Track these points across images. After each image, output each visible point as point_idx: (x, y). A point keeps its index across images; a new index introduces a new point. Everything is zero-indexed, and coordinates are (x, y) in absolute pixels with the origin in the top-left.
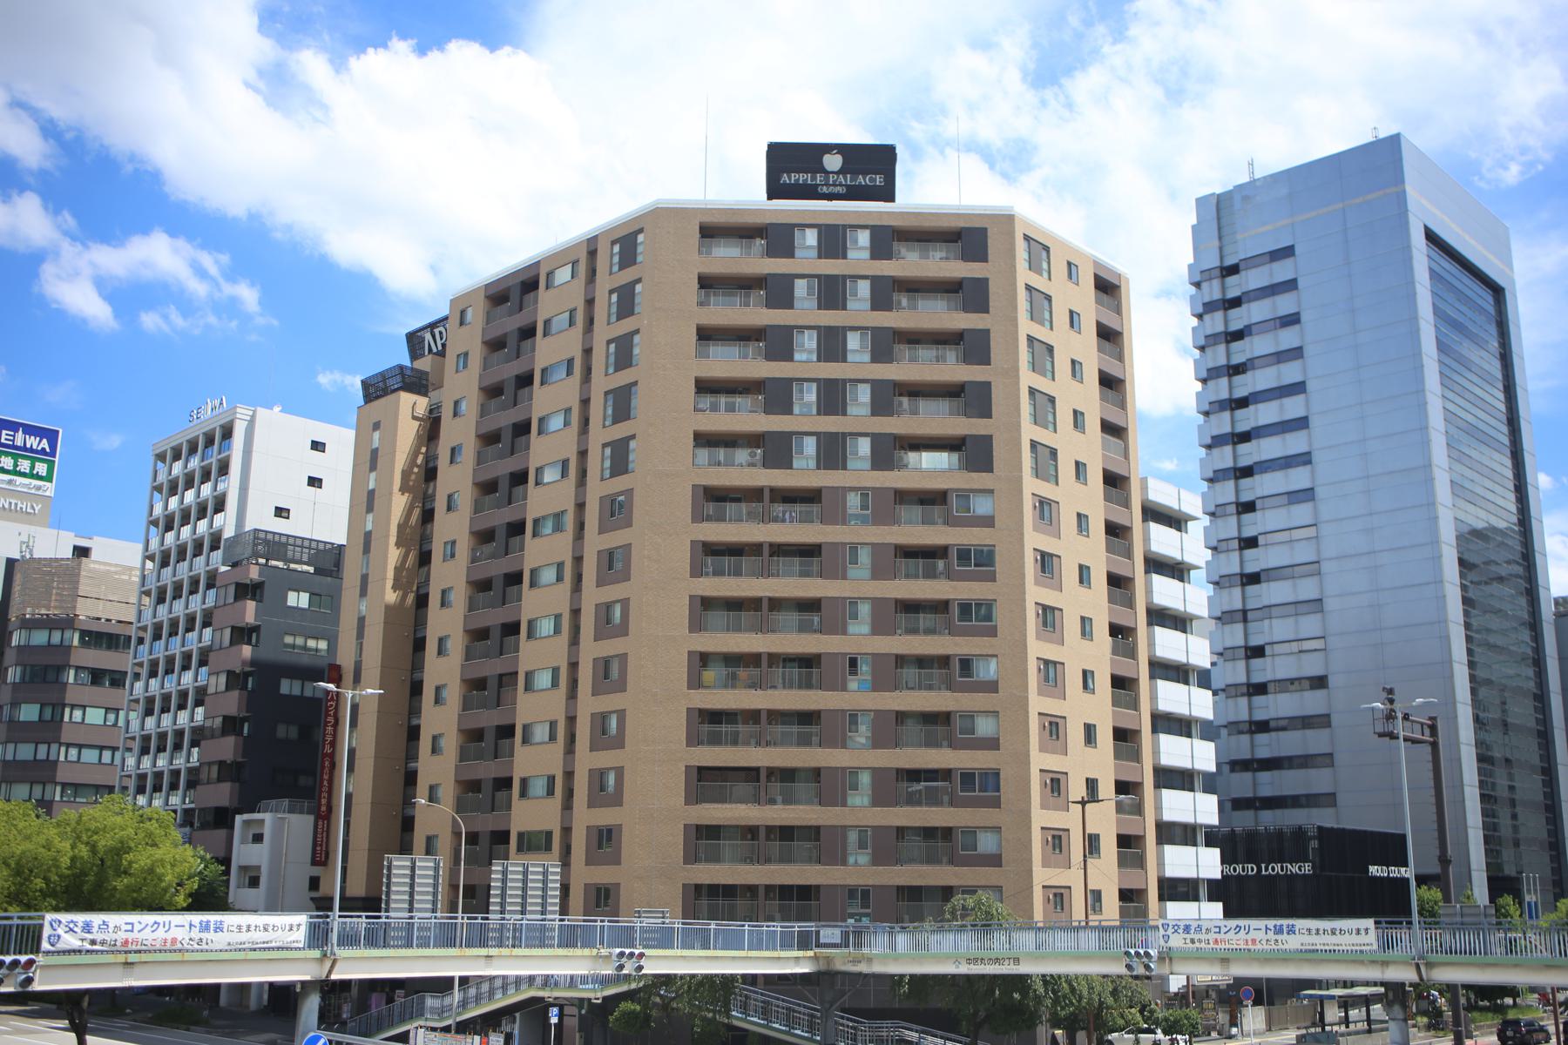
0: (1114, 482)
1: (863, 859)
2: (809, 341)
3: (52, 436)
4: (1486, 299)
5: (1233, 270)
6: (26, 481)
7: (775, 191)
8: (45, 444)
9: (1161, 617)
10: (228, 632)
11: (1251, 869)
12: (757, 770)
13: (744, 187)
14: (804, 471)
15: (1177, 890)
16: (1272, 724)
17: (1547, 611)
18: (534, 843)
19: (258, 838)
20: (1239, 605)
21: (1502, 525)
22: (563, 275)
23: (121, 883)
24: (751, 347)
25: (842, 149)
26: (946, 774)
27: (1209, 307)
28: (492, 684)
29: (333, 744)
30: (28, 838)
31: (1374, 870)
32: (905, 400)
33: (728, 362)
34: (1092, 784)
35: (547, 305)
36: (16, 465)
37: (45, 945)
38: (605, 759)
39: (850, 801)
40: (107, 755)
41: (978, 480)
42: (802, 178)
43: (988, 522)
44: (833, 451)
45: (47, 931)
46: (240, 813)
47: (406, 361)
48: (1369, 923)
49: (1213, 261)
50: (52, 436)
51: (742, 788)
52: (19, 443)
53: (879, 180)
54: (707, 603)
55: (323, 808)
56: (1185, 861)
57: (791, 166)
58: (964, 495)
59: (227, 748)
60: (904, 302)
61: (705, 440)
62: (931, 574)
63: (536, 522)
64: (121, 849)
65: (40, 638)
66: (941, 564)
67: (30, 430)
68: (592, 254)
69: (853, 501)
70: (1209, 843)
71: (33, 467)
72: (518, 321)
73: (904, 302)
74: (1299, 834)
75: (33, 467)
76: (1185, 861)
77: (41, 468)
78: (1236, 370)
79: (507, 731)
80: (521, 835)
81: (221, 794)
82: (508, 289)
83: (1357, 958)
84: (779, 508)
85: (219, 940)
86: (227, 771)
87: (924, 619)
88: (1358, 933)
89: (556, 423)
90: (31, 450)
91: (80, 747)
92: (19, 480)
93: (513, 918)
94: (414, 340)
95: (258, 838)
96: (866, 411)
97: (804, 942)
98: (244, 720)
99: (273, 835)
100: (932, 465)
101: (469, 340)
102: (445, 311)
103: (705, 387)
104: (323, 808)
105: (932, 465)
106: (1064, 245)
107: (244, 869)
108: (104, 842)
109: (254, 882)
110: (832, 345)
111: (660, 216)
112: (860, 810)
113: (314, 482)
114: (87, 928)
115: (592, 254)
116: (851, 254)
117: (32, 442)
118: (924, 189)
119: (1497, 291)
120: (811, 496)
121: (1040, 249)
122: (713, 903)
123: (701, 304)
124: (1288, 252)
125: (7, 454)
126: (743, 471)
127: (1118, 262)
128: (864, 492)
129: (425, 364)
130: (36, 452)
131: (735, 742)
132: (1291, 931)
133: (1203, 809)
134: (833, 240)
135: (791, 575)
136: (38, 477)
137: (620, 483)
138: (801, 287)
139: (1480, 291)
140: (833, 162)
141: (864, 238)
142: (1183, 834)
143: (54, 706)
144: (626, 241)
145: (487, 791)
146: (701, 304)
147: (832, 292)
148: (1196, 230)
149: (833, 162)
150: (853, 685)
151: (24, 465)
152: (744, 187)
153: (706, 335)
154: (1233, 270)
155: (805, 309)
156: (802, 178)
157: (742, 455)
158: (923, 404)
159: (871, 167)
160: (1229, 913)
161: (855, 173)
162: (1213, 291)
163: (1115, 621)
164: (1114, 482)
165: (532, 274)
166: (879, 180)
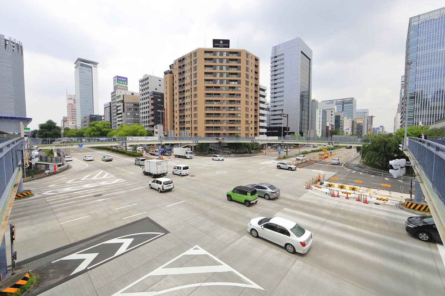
0: (256, 85)
1: (225, 130)
2: (219, 67)
4: (309, 60)
5: (276, 57)
7: (214, 46)
8: (126, 80)
9: (261, 102)
10: (151, 104)
11: (271, 131)
12: (213, 120)
13: (210, 46)
14: (218, 84)
15: (261, 133)
16: (151, 126)
17: (311, 101)
18: (188, 128)
19: (157, 128)
20: (274, 101)
21: (307, 91)
22: (187, 58)
23: (138, 133)
24: (211, 68)
25: (222, 40)
26: (234, 121)
27: (273, 62)
28: (182, 110)
29: (165, 117)
30: (127, 128)
32: (230, 75)
34: (252, 122)
35: (186, 62)
37: (127, 140)
38: (195, 119)
39: (224, 124)
41: (239, 85)
42: (218, 44)
43: (240, 91)
44: (221, 82)
45: (127, 139)
46: (155, 125)
47: (169, 69)
48: (277, 137)
49: (274, 56)
51: (211, 122)
53: (227, 45)
54: (207, 101)
56: (262, 130)
57: (216, 42)
58: (237, 87)
59: (152, 118)
60: (231, 62)
61: (206, 80)
62: (233, 97)
63: (186, 90)
64: (138, 129)
65: (128, 105)
66: (234, 96)
68: (191, 55)
69: (224, 88)
70: (265, 128)
72: (182, 64)
73: (231, 62)
74: (277, 127)
76: (262, 130)
78: (276, 71)
79: (184, 116)
81: (152, 123)
82: (181, 60)
83: (275, 141)
84: (215, 89)
85: (269, 139)
86: (153, 121)
87: (232, 103)
88: (276, 138)
89: (188, 78)
90: (124, 80)
93: (183, 137)
94: (170, 66)
95: (157, 128)
96: (225, 76)
97: (217, 139)
98: (154, 115)
99: (159, 128)
100: (233, 84)
101: (176, 67)
102: (173, 63)
103: (206, 73)
105: (233, 84)
106: (251, 54)
107: (156, 132)
108: (136, 129)
109: (157, 133)
110: (221, 68)
111: (199, 49)
112: (225, 125)
113: (160, 85)
114: (132, 138)
115: (191, 55)
116: (224, 55)
117: (124, 79)
118: (233, 46)
119: (310, 60)
120: (219, 87)
121: (248, 54)
122: (209, 135)
123: (205, 62)
124: (283, 54)
126: (211, 84)
127: (258, 56)
128: (225, 87)
129: (172, 70)
131: (210, 117)
132: (148, 138)
133: (265, 124)
134: (221, 53)
135: (216, 97)
136: (125, 84)
137: (196, 86)
138: (217, 60)
140: (221, 42)
141: (225, 53)
142: (262, 127)
143: (131, 113)
144: (195, 53)
145: (182, 123)
146: (205, 62)
147: (221, 60)
148: (55, 124)
149: (221, 42)
150: (224, 110)
151: (124, 83)
152: (210, 46)
153: (206, 66)
154: (276, 57)
155: (218, 63)
156: (218, 44)
157: (210, 82)
158: (233, 76)
159: (226, 43)
160: (267, 136)
161: (224, 44)
162: (274, 60)
164: (256, 85)
166: (227, 45)
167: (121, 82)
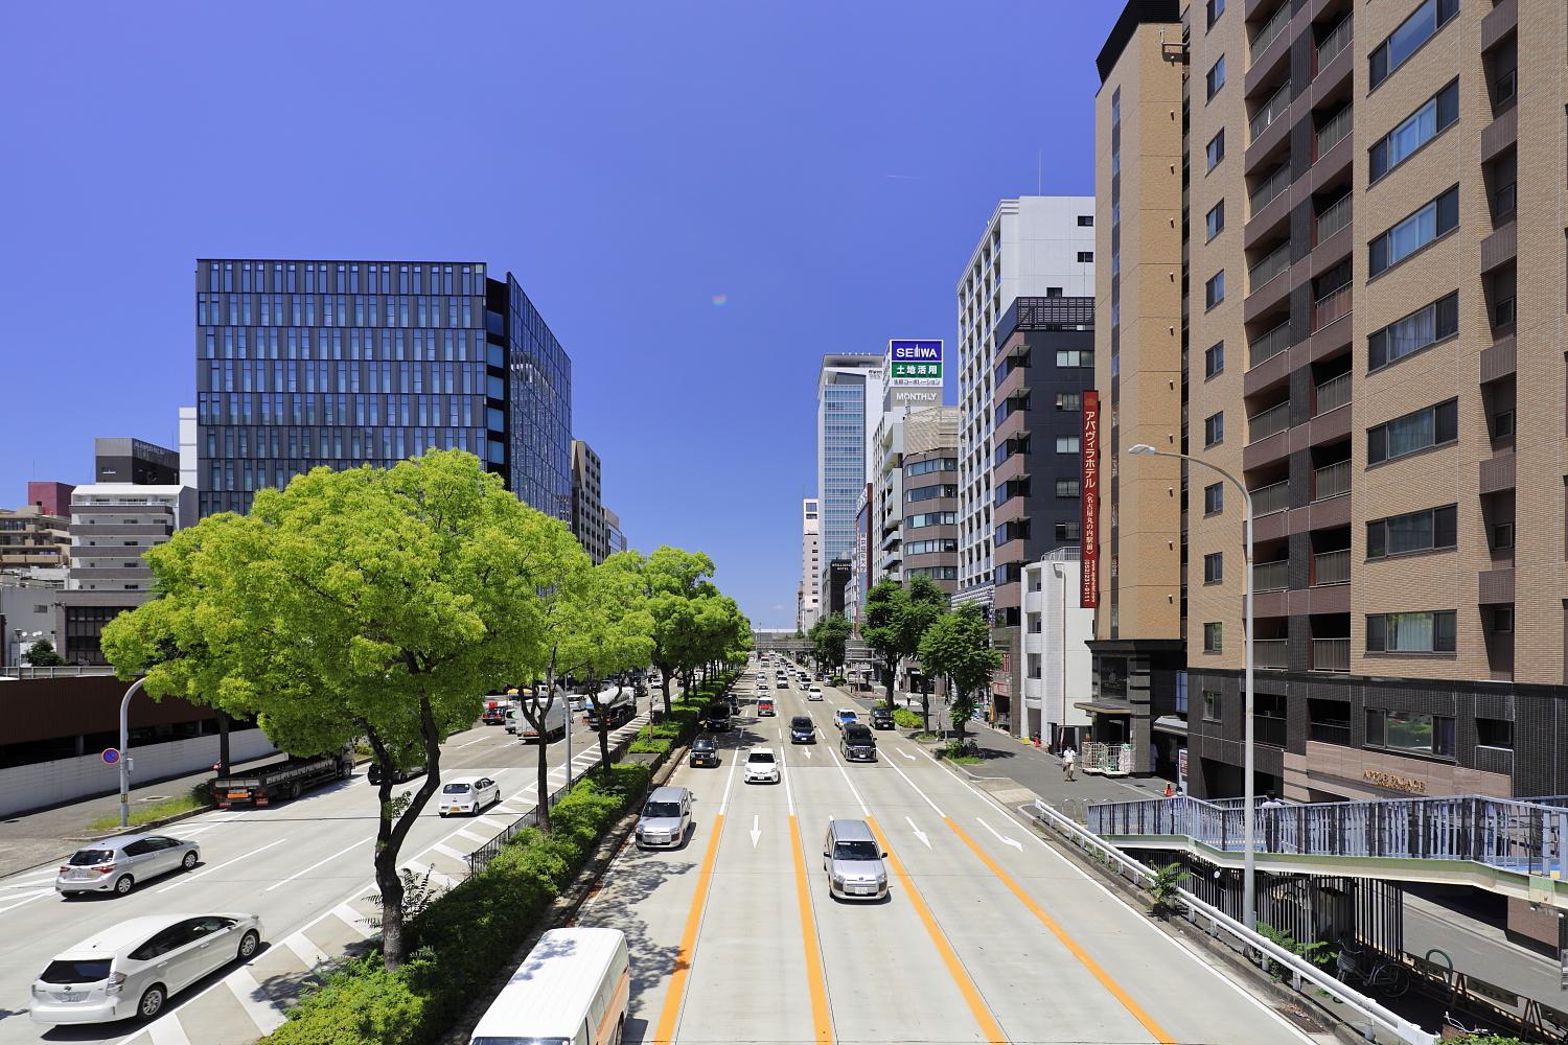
3: (936, 346)
6: (924, 379)
8: (933, 352)
31: (907, 818)
33: (780, 682)
36: (917, 370)
40: (929, 546)
50: (936, 346)
52: (917, 355)
55: (1090, 547)
67: (923, 345)
71: (927, 370)
75: (927, 370)
77: (933, 369)
80: (1375, 528)
86: (1016, 530)
90: (925, 358)
91: (914, 543)
92: (921, 380)
104: (1090, 547)
117: (925, 352)
125: (910, 364)
130: (928, 359)
136: (931, 375)
139: (1198, 952)
151: (922, 369)
163: (1258, 770)
165: (1262, 195)
167: (911, 369)
